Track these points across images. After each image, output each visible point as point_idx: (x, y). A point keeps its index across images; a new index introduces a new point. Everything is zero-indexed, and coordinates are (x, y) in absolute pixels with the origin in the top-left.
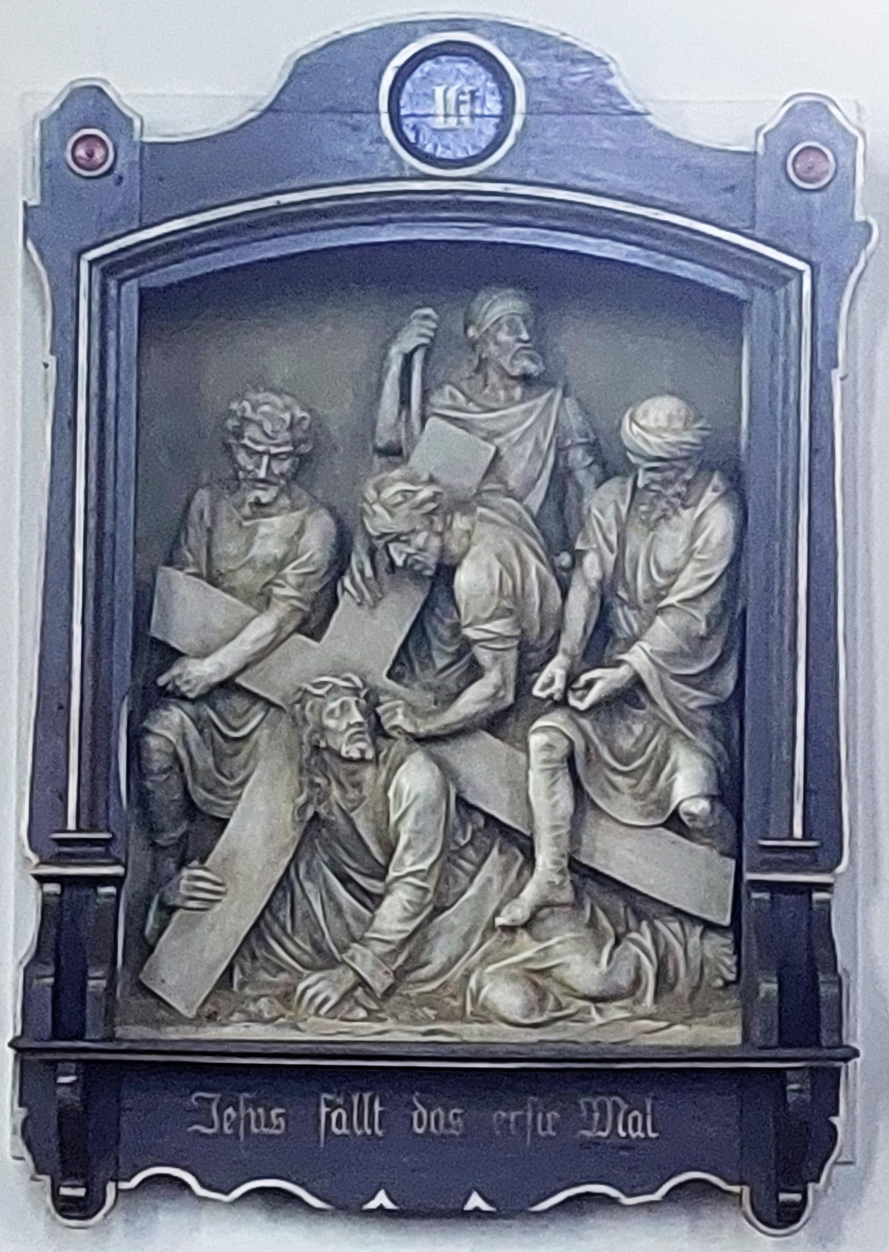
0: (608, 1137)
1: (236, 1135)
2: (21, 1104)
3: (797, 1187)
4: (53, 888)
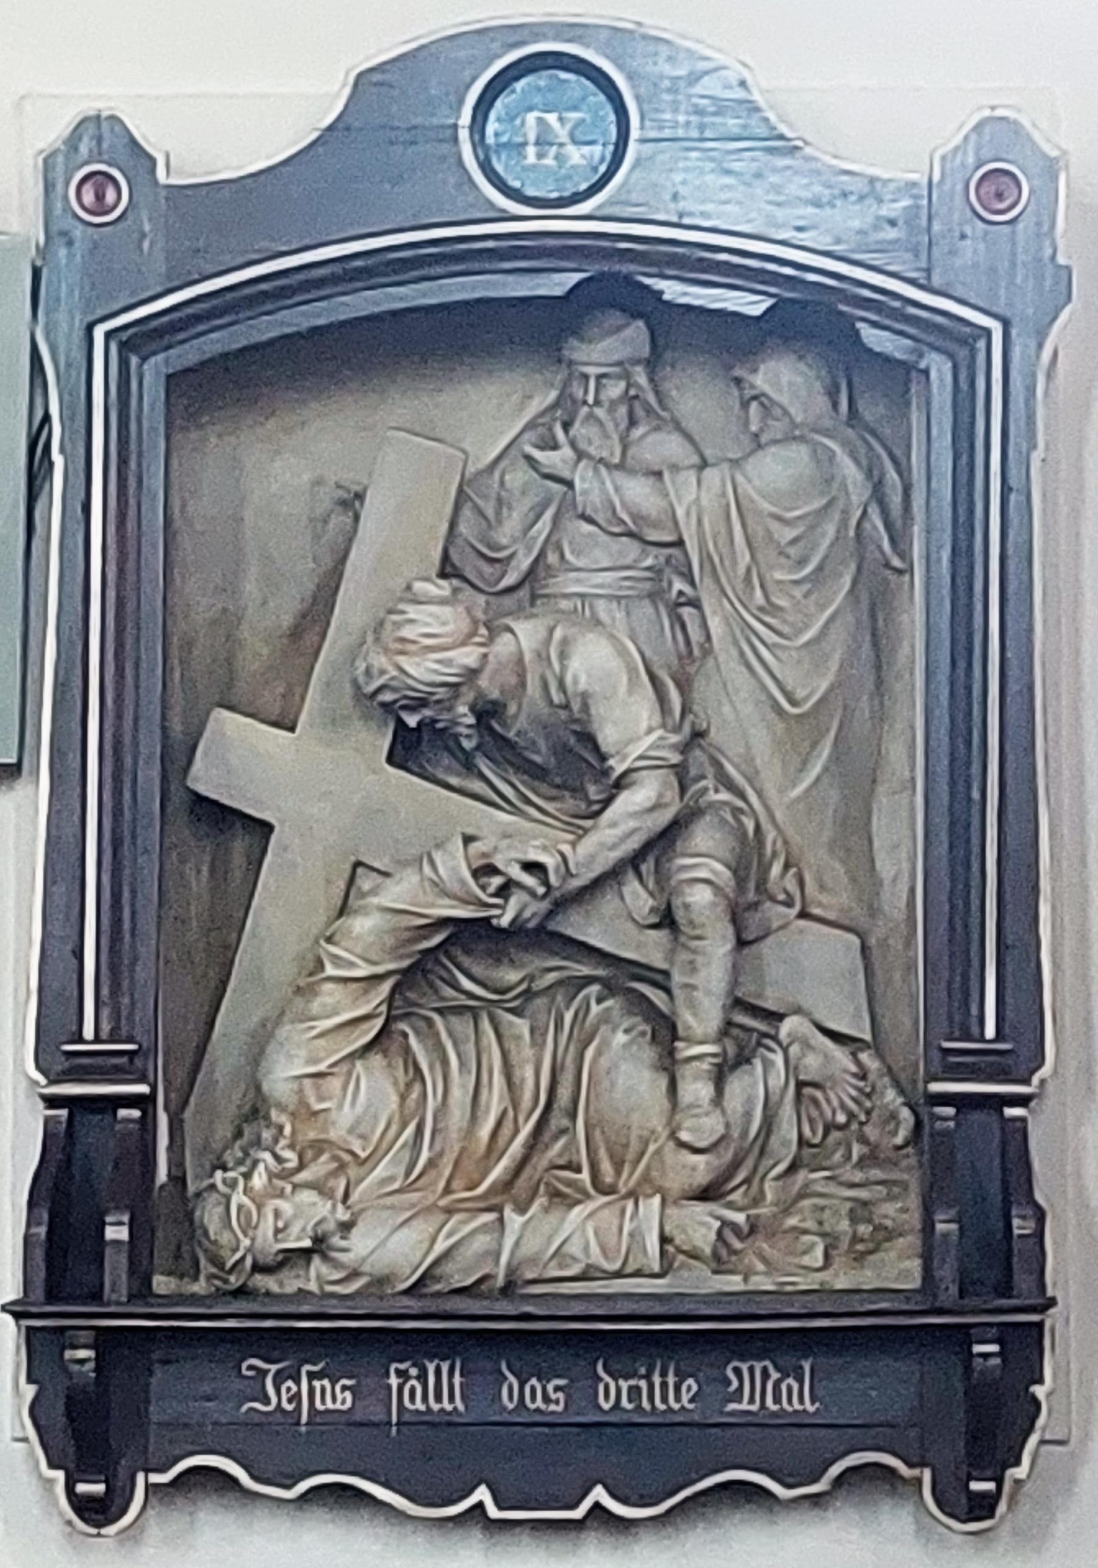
2: (30, 1380)
3: (989, 1473)
4: (63, 1113)
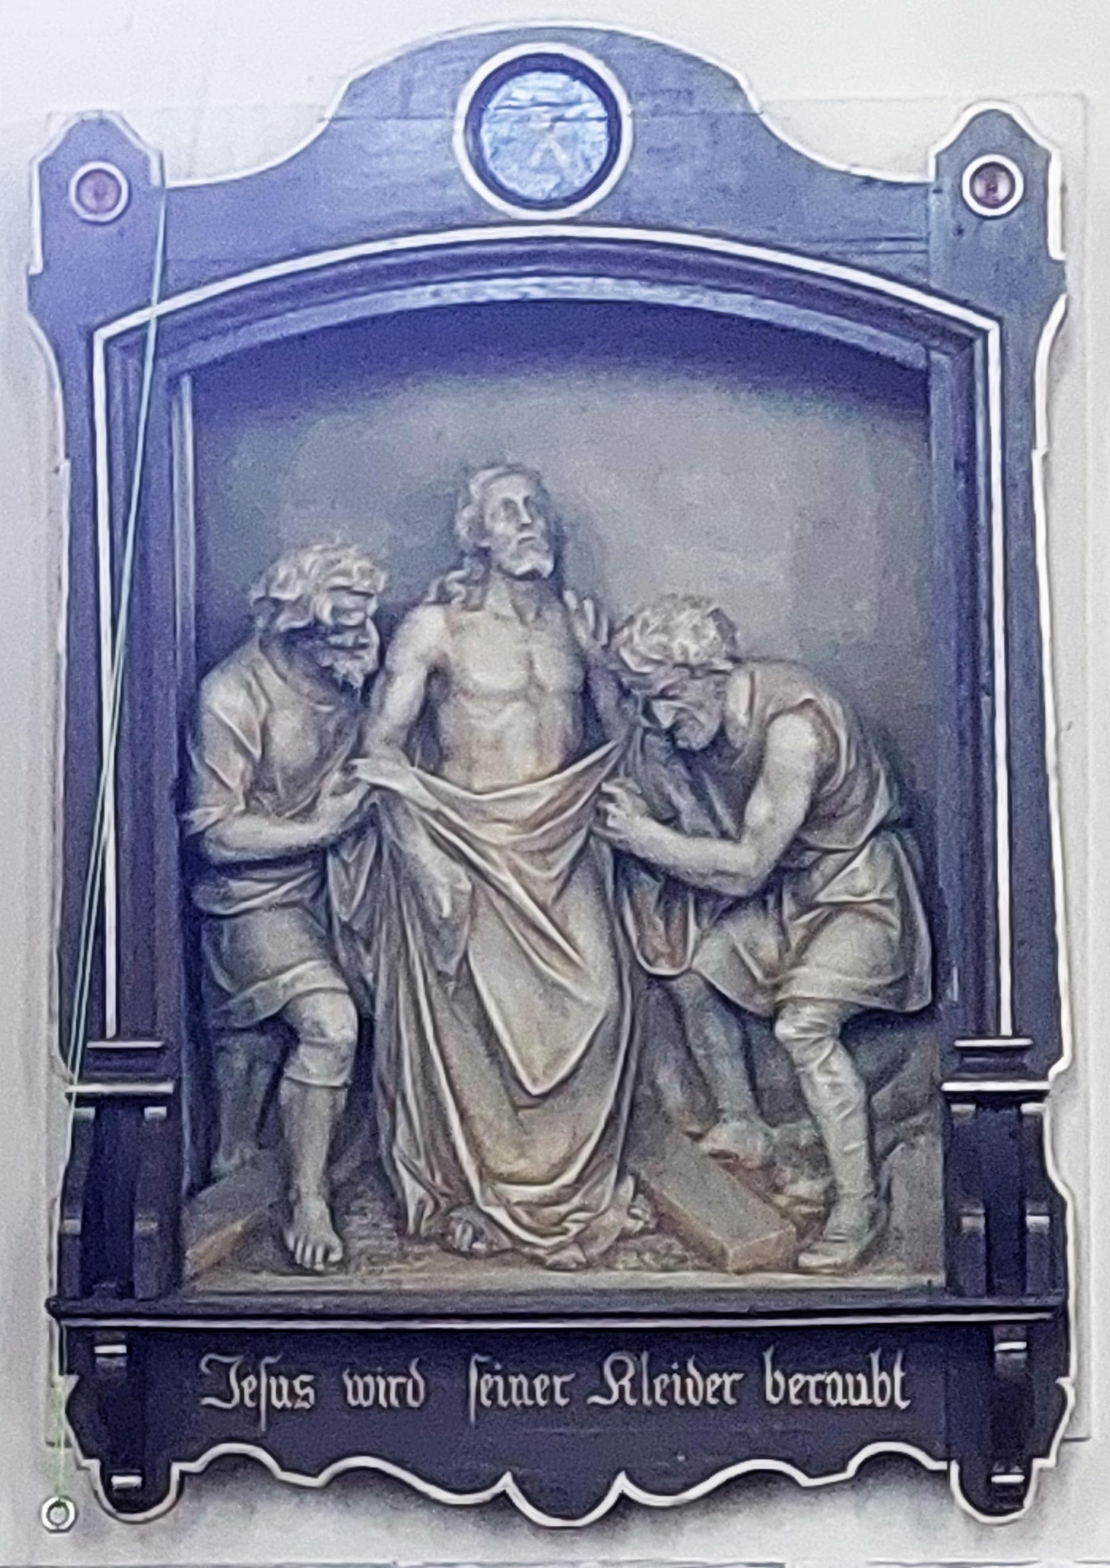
0: (777, 1405)
1: (258, 1407)
4: (90, 1112)
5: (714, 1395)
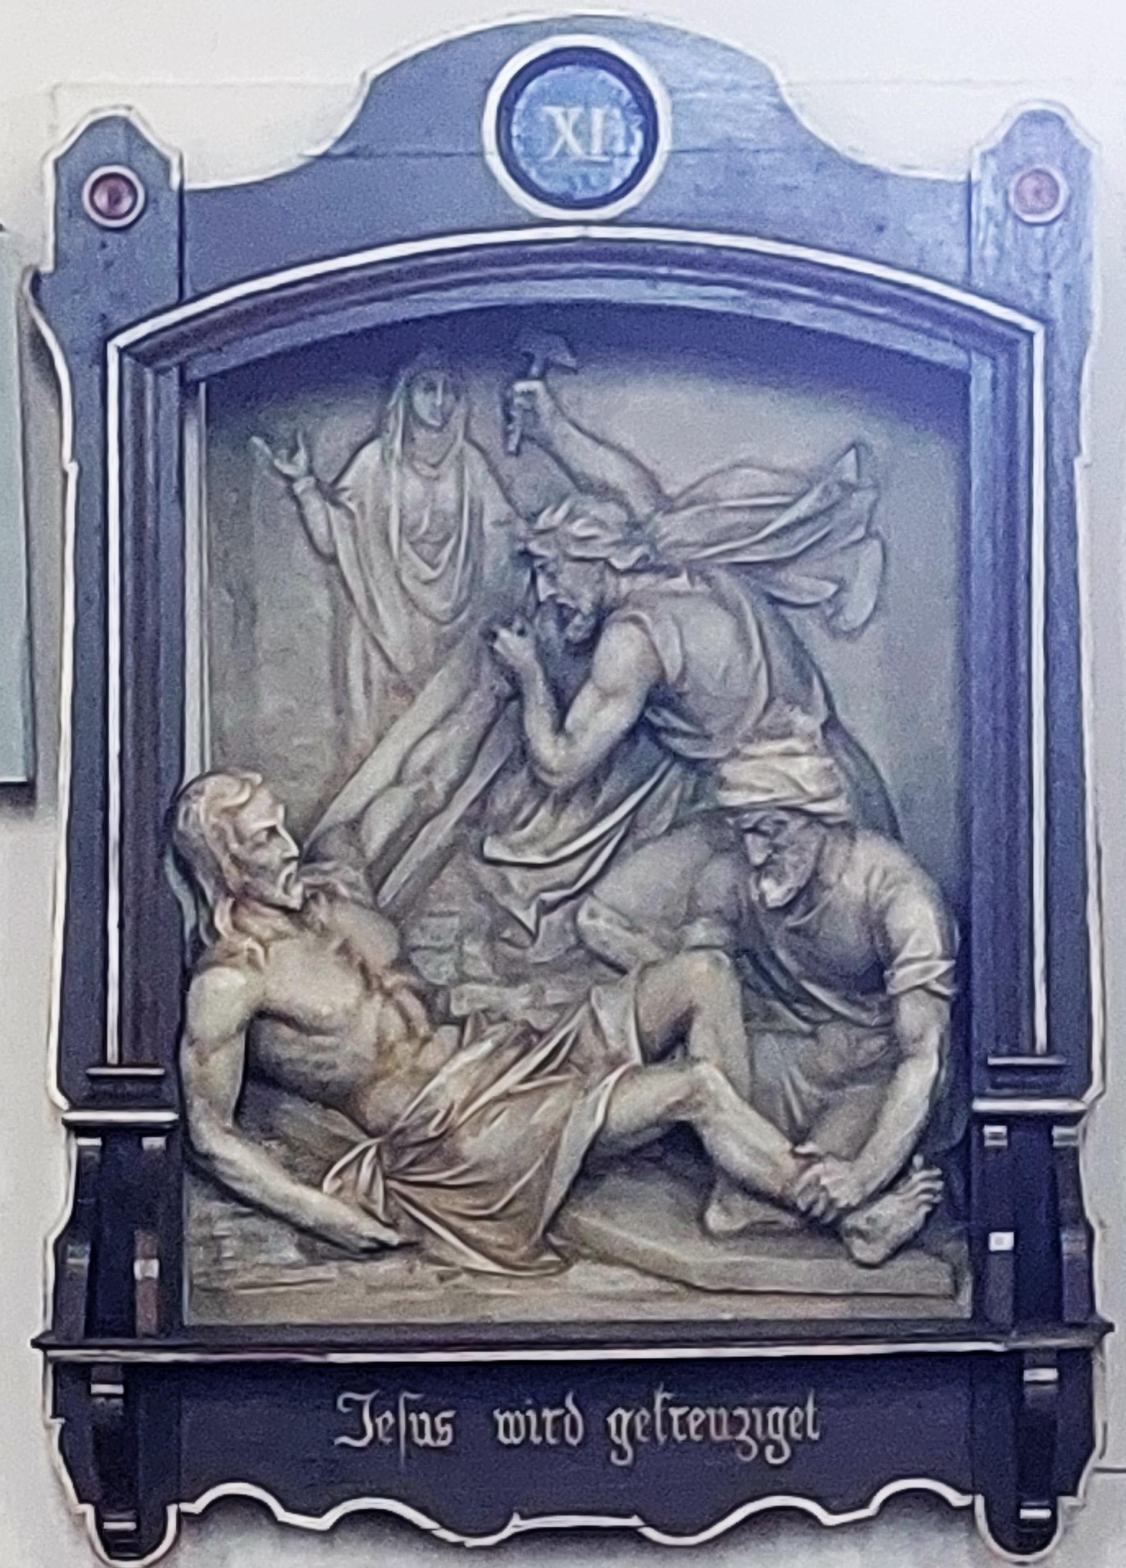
4: (97, 1142)
5: (387, 1435)
